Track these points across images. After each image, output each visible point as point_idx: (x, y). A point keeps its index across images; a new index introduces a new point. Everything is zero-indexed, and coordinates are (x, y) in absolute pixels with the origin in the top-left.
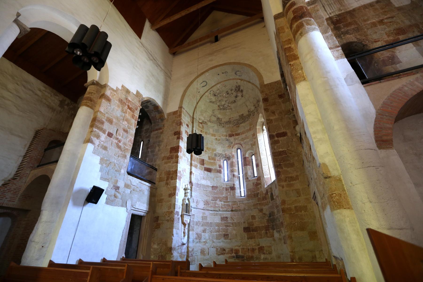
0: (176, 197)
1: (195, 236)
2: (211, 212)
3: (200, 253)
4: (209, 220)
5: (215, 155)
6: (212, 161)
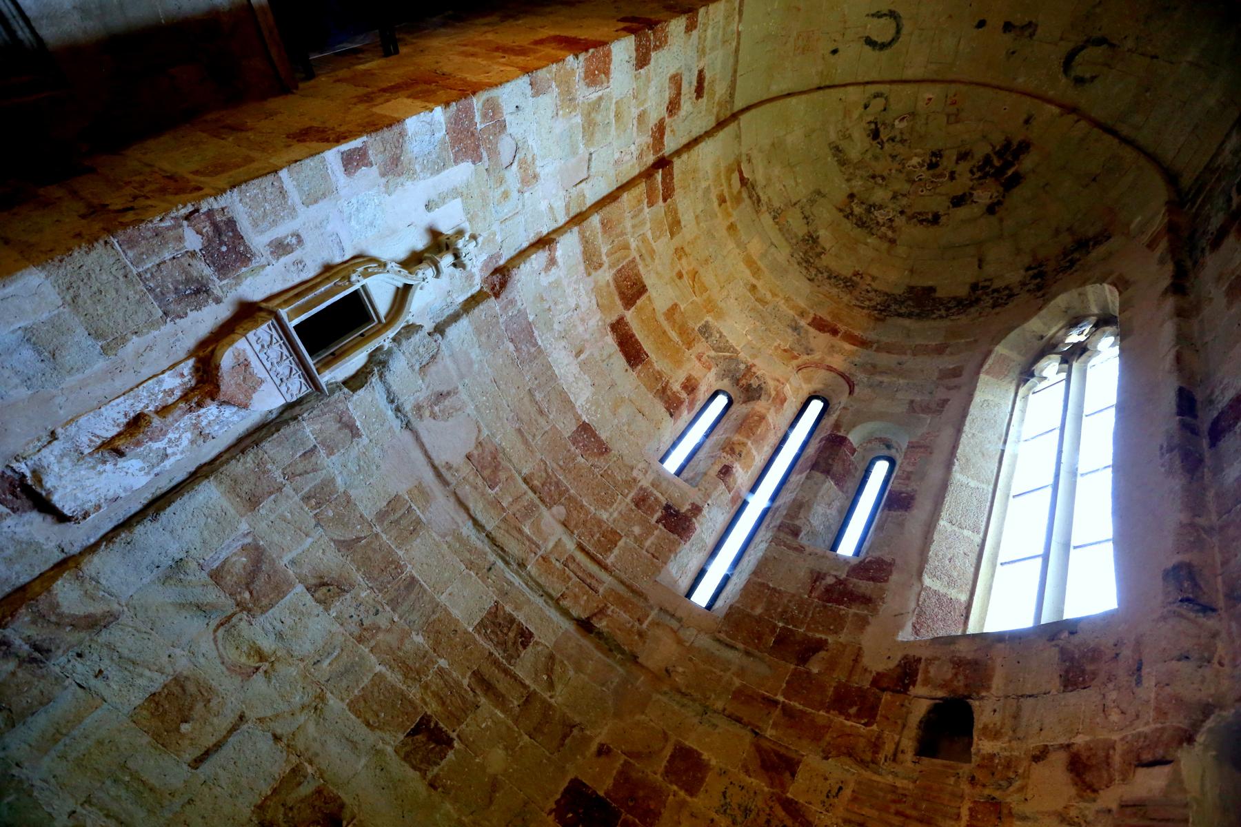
1: (228, 550)
2: (467, 529)
3: (137, 698)
4: (416, 557)
5: (706, 330)
6: (674, 335)
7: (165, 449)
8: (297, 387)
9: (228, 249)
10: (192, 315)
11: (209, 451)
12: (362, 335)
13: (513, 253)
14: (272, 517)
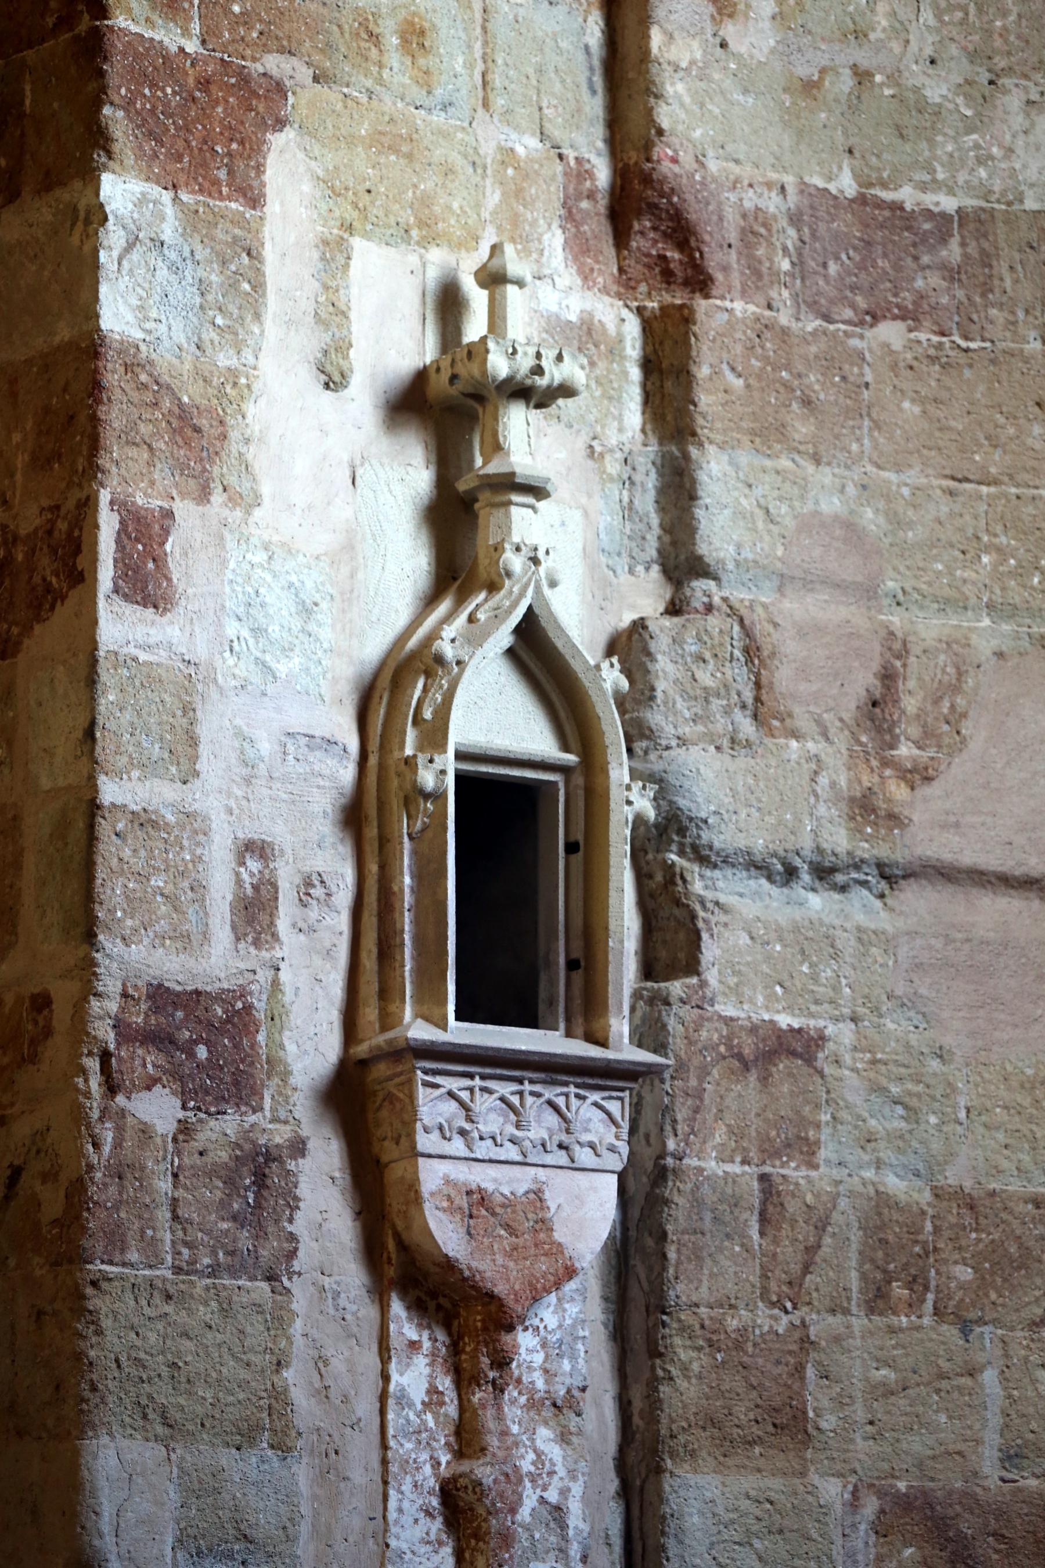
0: (119, 627)
7: (542, 1500)
8: (599, 1122)
9: (208, 1043)
10: (300, 1226)
11: (601, 1418)
12: (572, 848)
13: (595, 106)
14: (860, 1414)
